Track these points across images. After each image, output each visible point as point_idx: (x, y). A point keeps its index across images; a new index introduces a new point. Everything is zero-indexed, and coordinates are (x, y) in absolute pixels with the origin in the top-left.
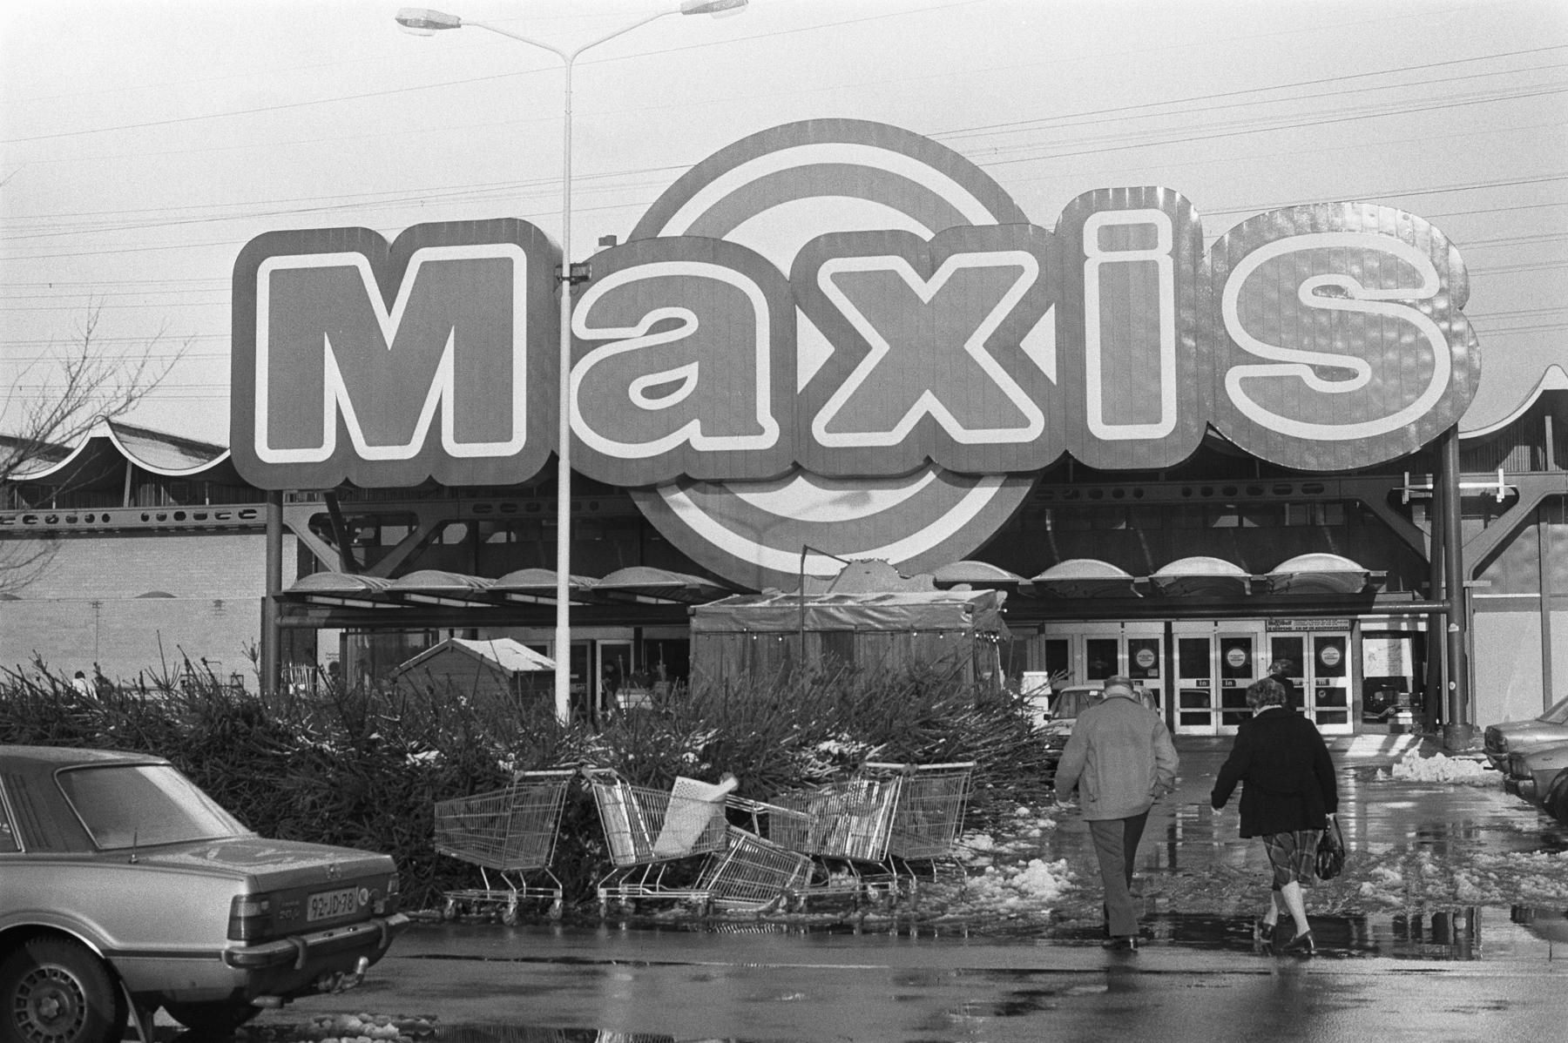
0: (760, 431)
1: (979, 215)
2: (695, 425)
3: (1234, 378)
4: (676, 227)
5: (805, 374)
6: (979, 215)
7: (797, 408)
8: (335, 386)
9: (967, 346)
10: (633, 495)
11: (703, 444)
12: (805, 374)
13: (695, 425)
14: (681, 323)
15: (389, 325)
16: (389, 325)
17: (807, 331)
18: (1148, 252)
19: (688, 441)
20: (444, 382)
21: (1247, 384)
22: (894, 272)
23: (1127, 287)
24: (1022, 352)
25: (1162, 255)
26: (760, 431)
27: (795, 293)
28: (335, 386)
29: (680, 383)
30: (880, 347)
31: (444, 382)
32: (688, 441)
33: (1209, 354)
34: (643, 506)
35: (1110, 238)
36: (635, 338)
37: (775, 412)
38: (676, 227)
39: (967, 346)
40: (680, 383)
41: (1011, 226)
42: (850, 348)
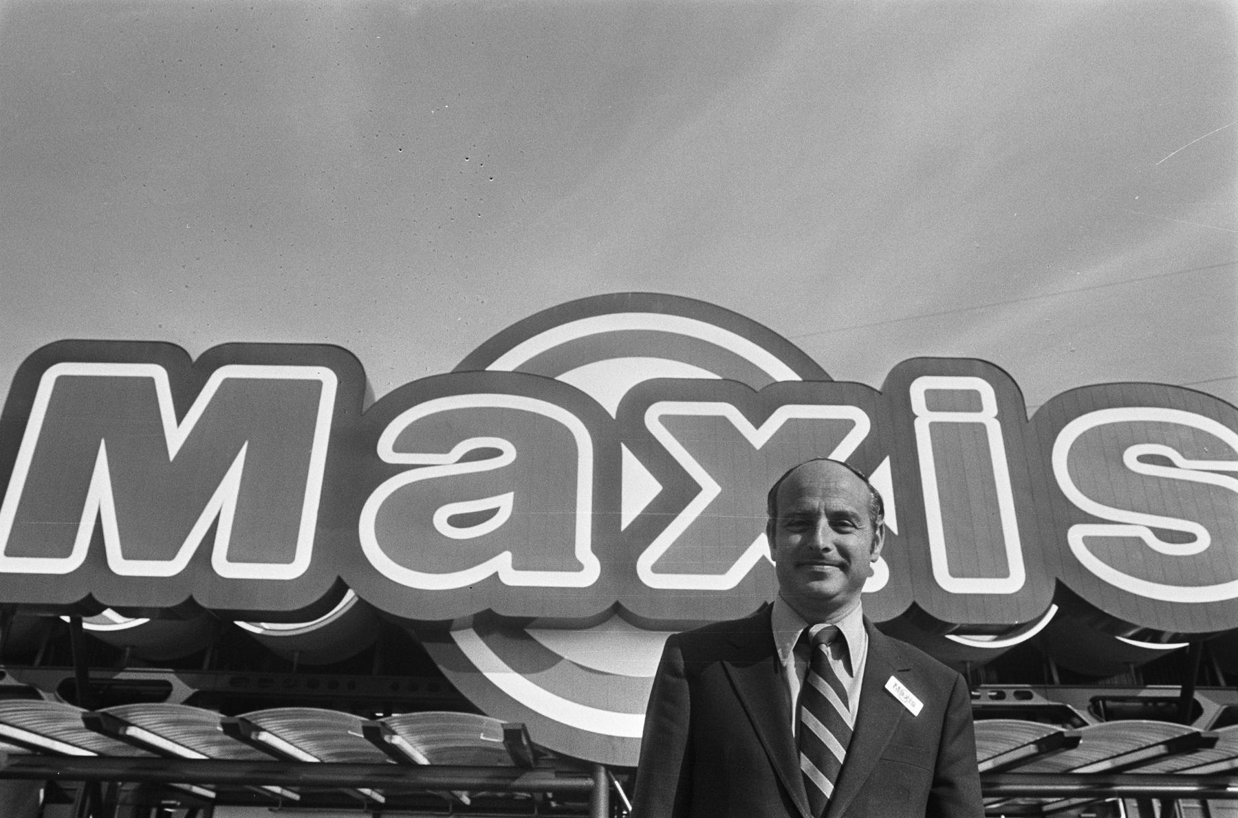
0: (579, 567)
1: (781, 372)
2: (506, 557)
3: (1076, 536)
4: (507, 363)
5: (631, 510)
6: (781, 372)
7: (619, 547)
8: (101, 493)
9: (718, 489)
10: (456, 635)
11: (513, 578)
12: (631, 510)
13: (506, 557)
14: (497, 453)
15: (176, 436)
16: (176, 436)
17: (631, 465)
18: (978, 414)
19: (496, 575)
20: (226, 498)
21: (1089, 542)
22: (790, 420)
23: (962, 448)
24: (660, 482)
25: (989, 415)
26: (579, 567)
27: (621, 431)
28: (101, 493)
29: (492, 513)
30: (710, 489)
31: (226, 498)
32: (496, 575)
33: (1047, 515)
34: (431, 649)
35: (936, 400)
36: (445, 465)
37: (596, 549)
38: (507, 363)
39: (718, 489)
40: (492, 513)
41: (816, 384)
42: (678, 490)
